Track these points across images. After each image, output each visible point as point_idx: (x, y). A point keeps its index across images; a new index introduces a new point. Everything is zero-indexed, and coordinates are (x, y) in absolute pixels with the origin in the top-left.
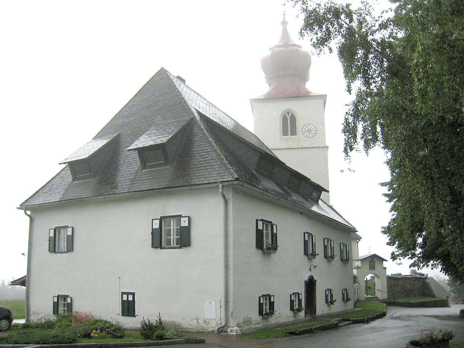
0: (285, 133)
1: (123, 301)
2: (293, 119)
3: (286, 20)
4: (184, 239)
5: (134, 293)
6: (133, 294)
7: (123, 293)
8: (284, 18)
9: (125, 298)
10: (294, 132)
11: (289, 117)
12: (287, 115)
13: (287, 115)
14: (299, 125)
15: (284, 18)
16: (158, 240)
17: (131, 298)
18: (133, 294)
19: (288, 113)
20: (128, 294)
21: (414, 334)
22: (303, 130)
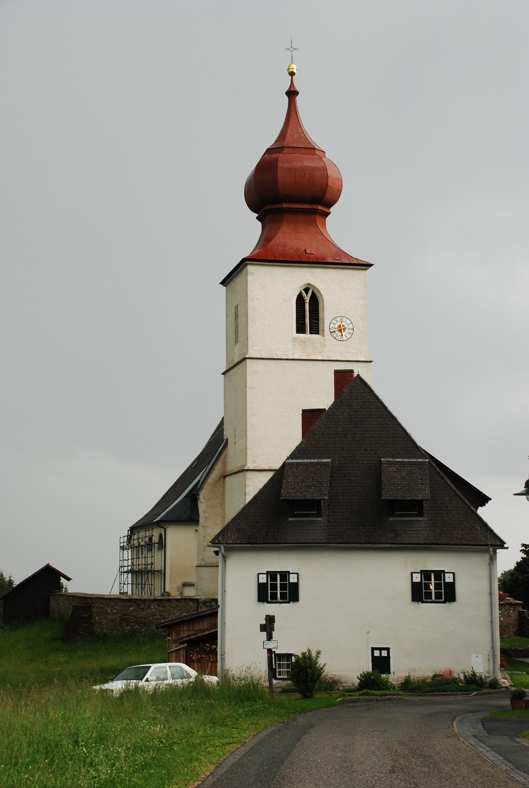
0: (301, 329)
1: (374, 658)
2: (315, 301)
3: (298, 88)
4: (448, 594)
5: (372, 648)
6: (388, 649)
7: (373, 649)
8: (292, 82)
9: (377, 653)
10: (315, 329)
11: (307, 299)
12: (304, 294)
13: (304, 294)
14: (328, 315)
15: (292, 82)
16: (419, 594)
17: (384, 653)
18: (388, 649)
19: (307, 290)
20: (381, 649)
21: (106, 686)
22: (332, 326)
